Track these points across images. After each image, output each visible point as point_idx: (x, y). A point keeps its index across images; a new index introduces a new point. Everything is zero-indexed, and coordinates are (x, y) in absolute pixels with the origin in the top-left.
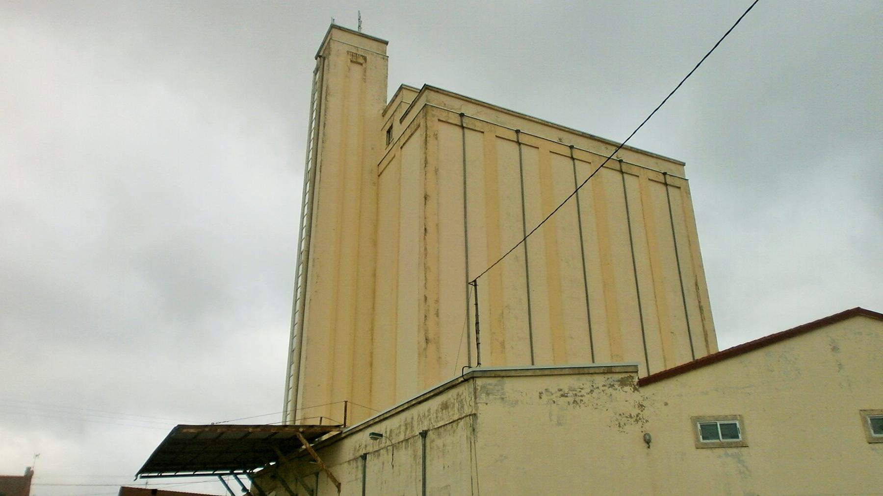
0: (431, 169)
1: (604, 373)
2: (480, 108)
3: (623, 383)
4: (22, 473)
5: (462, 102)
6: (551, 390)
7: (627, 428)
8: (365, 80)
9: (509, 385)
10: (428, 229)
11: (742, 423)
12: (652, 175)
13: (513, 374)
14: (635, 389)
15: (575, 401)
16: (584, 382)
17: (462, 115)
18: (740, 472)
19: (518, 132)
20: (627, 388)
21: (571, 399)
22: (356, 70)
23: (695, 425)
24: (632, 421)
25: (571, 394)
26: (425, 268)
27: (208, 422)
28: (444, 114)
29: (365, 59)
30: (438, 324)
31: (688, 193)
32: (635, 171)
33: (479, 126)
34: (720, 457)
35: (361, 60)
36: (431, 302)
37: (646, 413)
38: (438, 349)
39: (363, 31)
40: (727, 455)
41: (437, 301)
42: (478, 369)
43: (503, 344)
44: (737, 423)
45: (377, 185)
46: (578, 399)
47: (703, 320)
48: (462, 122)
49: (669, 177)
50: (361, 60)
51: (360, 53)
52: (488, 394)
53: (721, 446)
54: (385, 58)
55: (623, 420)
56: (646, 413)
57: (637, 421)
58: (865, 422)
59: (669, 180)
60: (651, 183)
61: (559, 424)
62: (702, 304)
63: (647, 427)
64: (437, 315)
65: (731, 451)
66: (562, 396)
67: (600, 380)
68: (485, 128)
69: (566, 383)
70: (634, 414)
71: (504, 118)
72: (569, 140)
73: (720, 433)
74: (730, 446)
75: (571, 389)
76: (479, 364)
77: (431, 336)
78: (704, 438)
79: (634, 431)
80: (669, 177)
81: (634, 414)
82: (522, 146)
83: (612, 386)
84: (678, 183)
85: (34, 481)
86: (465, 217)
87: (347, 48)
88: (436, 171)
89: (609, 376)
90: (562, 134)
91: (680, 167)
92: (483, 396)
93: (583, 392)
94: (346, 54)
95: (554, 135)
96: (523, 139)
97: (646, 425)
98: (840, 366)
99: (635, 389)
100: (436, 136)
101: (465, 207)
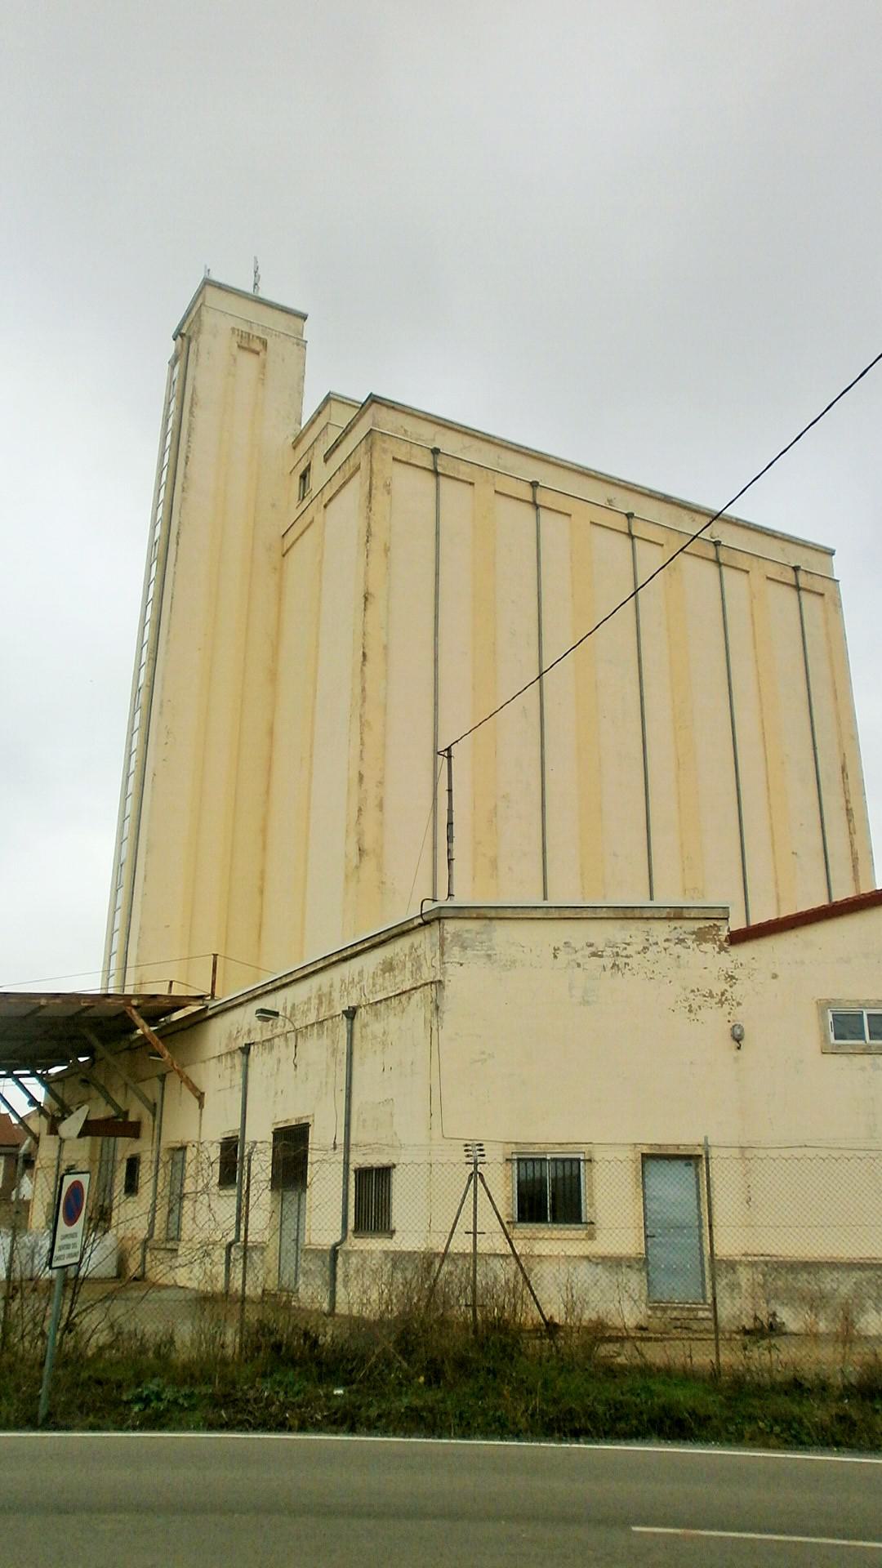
0: (375, 545)
2: (467, 440)
3: (701, 936)
7: (702, 1015)
9: (503, 933)
12: (773, 571)
14: (722, 949)
16: (634, 932)
19: (534, 485)
21: (608, 962)
22: (248, 362)
26: (362, 725)
29: (265, 343)
30: (381, 824)
31: (838, 604)
33: (464, 472)
34: (863, 1069)
35: (257, 346)
36: (370, 783)
37: (738, 991)
38: (380, 868)
39: (265, 293)
43: (494, 863)
45: (280, 571)
46: (620, 961)
48: (435, 463)
50: (257, 346)
51: (257, 332)
52: (464, 948)
53: (867, 1051)
54: (301, 344)
55: (700, 1000)
56: (738, 991)
57: (721, 1003)
61: (585, 1003)
63: (739, 1015)
64: (381, 806)
66: (594, 954)
69: (602, 933)
70: (717, 991)
71: (510, 460)
77: (368, 844)
79: (716, 1021)
81: (717, 991)
83: (681, 941)
87: (232, 323)
89: (674, 924)
90: (612, 492)
91: (827, 557)
92: (456, 950)
93: (630, 950)
95: (598, 493)
96: (543, 498)
99: (722, 949)
100: (388, 487)
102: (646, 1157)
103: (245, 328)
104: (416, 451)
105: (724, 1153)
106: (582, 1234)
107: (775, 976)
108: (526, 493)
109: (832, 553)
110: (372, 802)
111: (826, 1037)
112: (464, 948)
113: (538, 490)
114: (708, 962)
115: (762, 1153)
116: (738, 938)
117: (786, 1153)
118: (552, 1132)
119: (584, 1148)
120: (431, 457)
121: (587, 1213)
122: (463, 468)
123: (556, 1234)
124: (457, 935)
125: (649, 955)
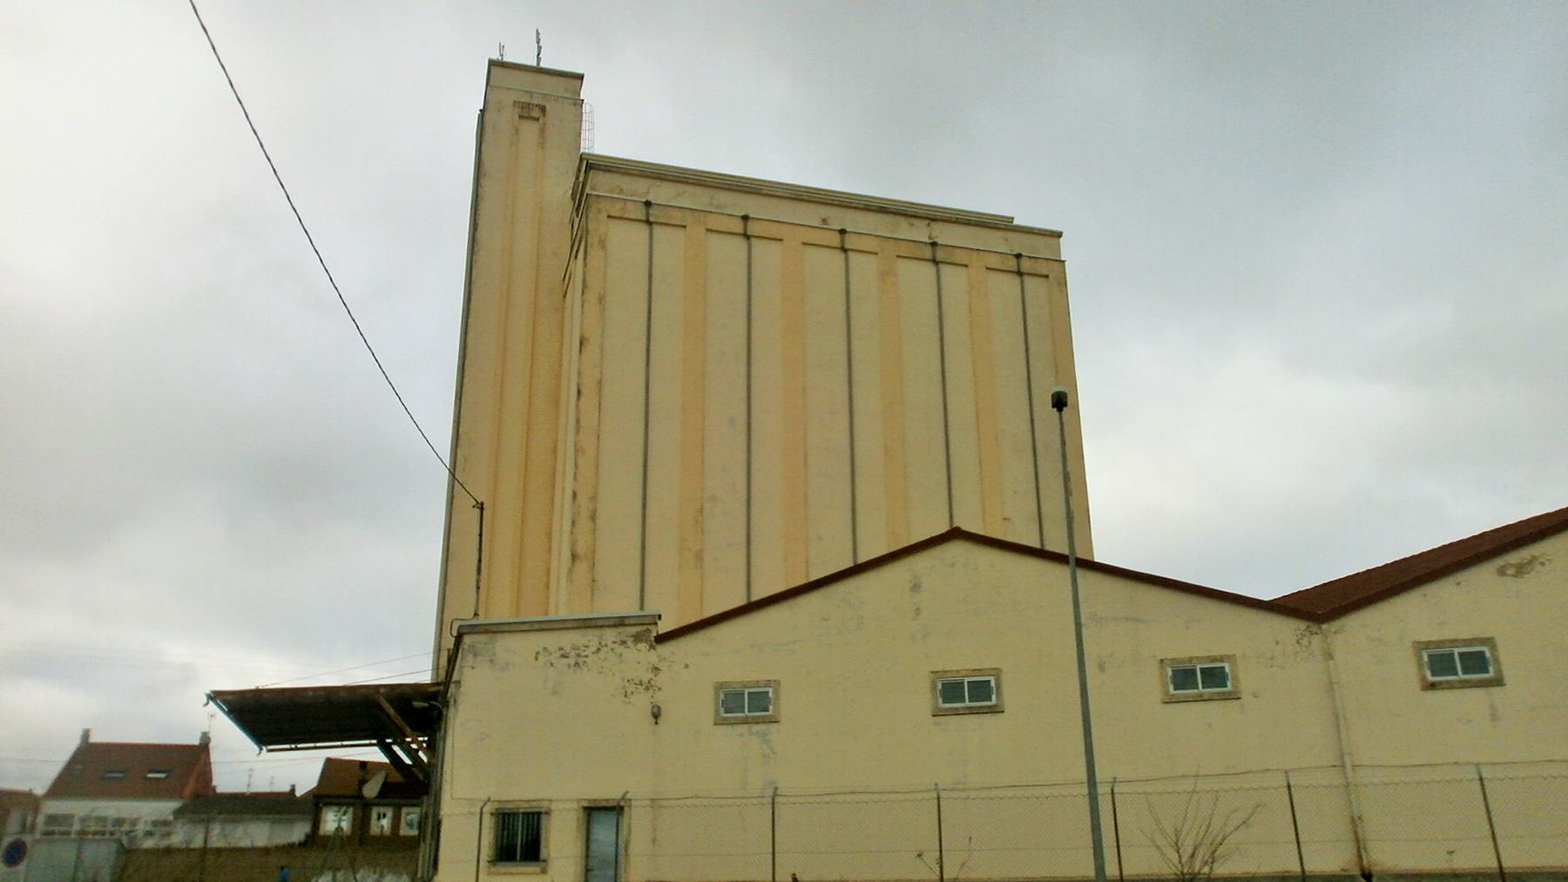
0: (592, 296)
1: (615, 626)
2: (681, 188)
3: (638, 638)
4: (195, 741)
5: (649, 182)
6: (551, 649)
7: (633, 699)
8: (542, 145)
10: (583, 390)
11: (776, 692)
12: (993, 261)
13: (506, 628)
14: (652, 647)
15: (577, 664)
16: (589, 638)
17: (648, 204)
18: (764, 755)
19: (745, 218)
20: (643, 646)
21: (571, 661)
22: (529, 130)
23: (717, 694)
24: (641, 688)
25: (573, 653)
27: (252, 687)
28: (618, 206)
29: (543, 109)
31: (1063, 283)
32: (961, 257)
33: (676, 217)
34: (742, 735)
36: (583, 500)
37: (660, 679)
40: (751, 733)
41: (594, 498)
42: (475, 622)
43: (699, 556)
44: (770, 690)
46: (581, 660)
47: (1068, 492)
48: (648, 214)
49: (1031, 259)
50: (536, 113)
52: (475, 655)
55: (631, 688)
56: (660, 679)
58: (934, 687)
59: (1026, 265)
60: (991, 273)
61: (554, 693)
62: (1069, 469)
64: (593, 517)
65: (756, 728)
66: (563, 656)
67: (610, 635)
68: (689, 219)
69: (569, 639)
70: (645, 680)
71: (724, 198)
72: (840, 218)
73: (746, 705)
74: (756, 721)
75: (575, 648)
76: (476, 614)
77: (581, 549)
78: (1223, 668)
79: (642, 701)
80: (1031, 259)
81: (645, 680)
82: (754, 242)
83: (624, 642)
84: (1042, 268)
85: (211, 745)
86: (648, 364)
87: (514, 96)
88: (601, 299)
89: (621, 629)
90: (825, 211)
91: (1051, 241)
92: (470, 657)
93: (588, 652)
94: (528, 101)
95: (811, 214)
96: (754, 228)
97: (659, 694)
98: (918, 611)
99: (652, 647)
101: (648, 350)
102: (586, 808)
103: (526, 99)
104: (630, 206)
105: (1129, 788)
106: (538, 869)
107: (687, 666)
108: (737, 226)
109: (1059, 235)
110: (584, 513)
111: (717, 712)
112: (475, 655)
113: (750, 224)
114: (640, 657)
115: (665, 803)
116: (662, 639)
117: (983, 794)
118: (521, 792)
119: (545, 804)
120: (643, 210)
121: (543, 854)
122: (675, 213)
123: (513, 870)
124: (472, 646)
125: (601, 654)
